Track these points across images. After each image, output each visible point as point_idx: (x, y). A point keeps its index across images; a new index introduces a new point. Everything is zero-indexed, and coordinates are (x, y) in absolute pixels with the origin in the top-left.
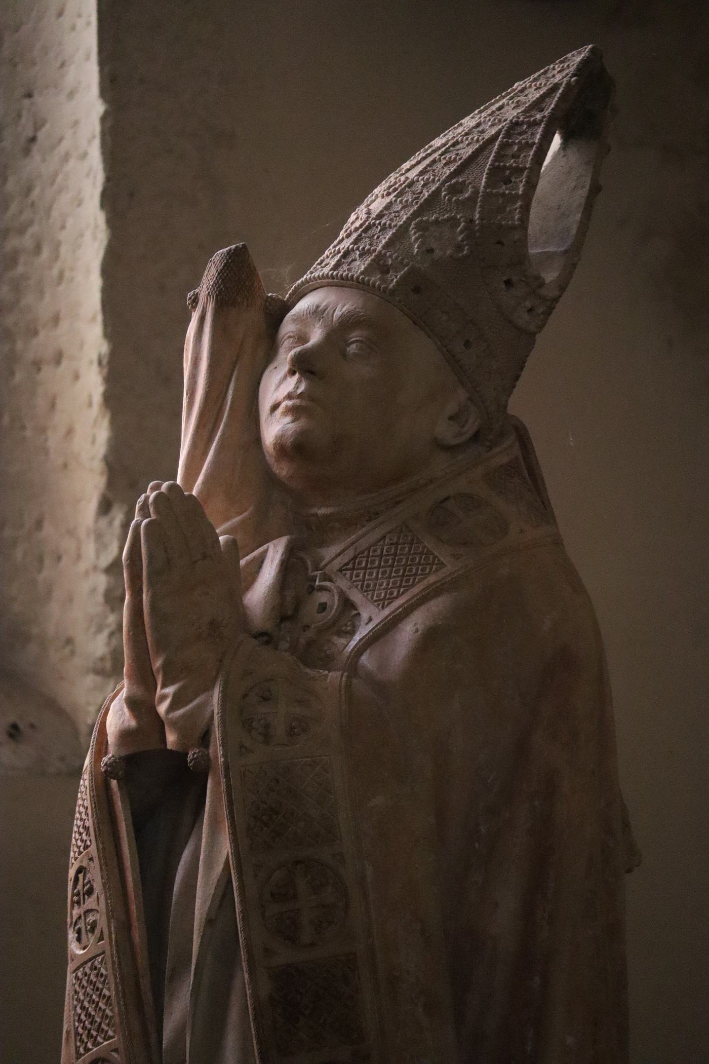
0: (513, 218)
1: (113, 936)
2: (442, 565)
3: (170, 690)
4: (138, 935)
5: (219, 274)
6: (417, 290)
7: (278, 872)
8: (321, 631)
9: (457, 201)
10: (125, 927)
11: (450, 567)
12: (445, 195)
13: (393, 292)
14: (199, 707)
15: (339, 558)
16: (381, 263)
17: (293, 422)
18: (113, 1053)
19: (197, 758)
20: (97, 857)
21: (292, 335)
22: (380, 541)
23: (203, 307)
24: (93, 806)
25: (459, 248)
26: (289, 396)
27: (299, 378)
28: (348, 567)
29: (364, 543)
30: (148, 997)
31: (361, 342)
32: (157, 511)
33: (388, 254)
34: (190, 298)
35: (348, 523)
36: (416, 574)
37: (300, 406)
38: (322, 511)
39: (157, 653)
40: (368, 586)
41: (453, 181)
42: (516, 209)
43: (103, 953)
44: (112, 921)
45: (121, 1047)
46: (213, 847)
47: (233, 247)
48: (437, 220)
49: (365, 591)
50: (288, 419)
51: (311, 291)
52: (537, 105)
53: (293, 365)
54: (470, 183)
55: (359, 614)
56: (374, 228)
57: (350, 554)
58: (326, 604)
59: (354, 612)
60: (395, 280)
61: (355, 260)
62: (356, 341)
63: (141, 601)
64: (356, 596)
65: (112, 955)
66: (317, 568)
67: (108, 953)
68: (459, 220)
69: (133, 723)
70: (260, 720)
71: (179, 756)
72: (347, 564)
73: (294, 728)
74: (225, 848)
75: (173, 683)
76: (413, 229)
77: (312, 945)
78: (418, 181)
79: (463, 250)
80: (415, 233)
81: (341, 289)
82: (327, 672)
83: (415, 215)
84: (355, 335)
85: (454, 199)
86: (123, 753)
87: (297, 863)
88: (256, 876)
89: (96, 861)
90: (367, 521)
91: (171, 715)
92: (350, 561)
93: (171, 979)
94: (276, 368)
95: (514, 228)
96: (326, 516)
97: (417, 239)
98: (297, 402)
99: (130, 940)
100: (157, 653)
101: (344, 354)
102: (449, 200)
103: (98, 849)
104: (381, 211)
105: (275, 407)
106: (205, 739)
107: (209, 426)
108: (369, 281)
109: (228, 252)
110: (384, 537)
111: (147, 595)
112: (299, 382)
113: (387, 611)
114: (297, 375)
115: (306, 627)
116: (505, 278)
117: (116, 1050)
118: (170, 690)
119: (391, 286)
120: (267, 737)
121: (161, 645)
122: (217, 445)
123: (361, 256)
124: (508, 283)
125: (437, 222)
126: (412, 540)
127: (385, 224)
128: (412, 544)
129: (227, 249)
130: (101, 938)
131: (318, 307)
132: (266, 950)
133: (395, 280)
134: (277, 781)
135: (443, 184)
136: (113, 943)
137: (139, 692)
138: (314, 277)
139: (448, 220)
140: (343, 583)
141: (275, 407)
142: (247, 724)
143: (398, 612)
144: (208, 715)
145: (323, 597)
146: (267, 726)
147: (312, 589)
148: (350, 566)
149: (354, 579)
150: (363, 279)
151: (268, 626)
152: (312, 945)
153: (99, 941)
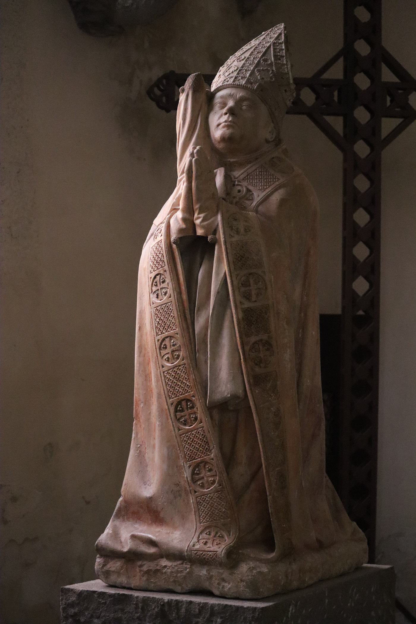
0: (285, 71)
1: (176, 296)
2: (279, 179)
3: (202, 215)
4: (185, 297)
5: (193, 82)
6: (262, 90)
7: (243, 277)
8: (240, 198)
9: (267, 64)
10: (180, 293)
11: (281, 180)
12: (263, 62)
13: (256, 90)
14: (213, 222)
15: (242, 175)
16: (250, 81)
17: (227, 130)
18: (176, 335)
19: (212, 238)
20: (168, 270)
21: (221, 102)
22: (255, 170)
23: (188, 92)
24: (167, 253)
25: (271, 78)
26: (226, 122)
27: (229, 116)
28: (246, 178)
29: (250, 171)
30: (188, 316)
31: (247, 105)
32: (197, 155)
33: (251, 78)
34: (181, 91)
35: (241, 165)
36: (271, 181)
37: (230, 125)
38: (232, 160)
39: (197, 203)
40: (254, 185)
41: (263, 58)
42: (285, 68)
43: (171, 302)
44: (175, 291)
45: (179, 332)
46: (218, 268)
47: (197, 73)
48: (263, 69)
49: (254, 186)
50: (225, 129)
51: (223, 89)
52: (278, 38)
53: (228, 111)
54: (269, 59)
55: (253, 194)
56: (242, 70)
57: (245, 174)
58: (240, 190)
59: (252, 193)
60: (255, 87)
61: (240, 80)
62: (245, 105)
63: (191, 185)
64: (250, 188)
65: (175, 303)
66: (235, 178)
67: (173, 302)
68: (269, 70)
69: (184, 226)
70: (235, 226)
71: (203, 238)
72: (245, 177)
73: (246, 229)
74: (225, 268)
75: (202, 213)
76: (256, 71)
77: (255, 301)
78: (250, 57)
79: (273, 79)
80: (257, 73)
81: (237, 88)
82: (246, 212)
83: (256, 67)
84: (245, 103)
85: (266, 63)
86: (180, 236)
87: (250, 274)
88: (237, 278)
89: (168, 272)
90: (247, 164)
91: (202, 224)
92: (246, 176)
93: (199, 310)
94: (215, 113)
95: (286, 74)
96: (234, 162)
97: (259, 75)
98: (229, 123)
99: (181, 297)
100: (197, 203)
101: (241, 109)
102: (264, 63)
103: (169, 267)
104: (242, 66)
105: (219, 125)
106: (215, 232)
107: (192, 131)
108: (248, 86)
109: (196, 75)
110: (256, 169)
111: (195, 183)
112: (229, 117)
113: (264, 193)
114: (228, 115)
115: (234, 197)
116: (285, 89)
117: (177, 334)
118: (202, 215)
119: (255, 88)
120: (238, 232)
121: (198, 200)
122: (196, 136)
123: (242, 78)
124: (285, 91)
125: (263, 70)
126: (266, 170)
127: (246, 69)
128: (266, 172)
129: (195, 74)
130: (170, 297)
131: (230, 93)
132: (241, 302)
133: (255, 87)
134: (243, 247)
135: (260, 59)
136: (176, 299)
137: (187, 216)
138: (224, 85)
139: (266, 70)
140: (245, 184)
141: (219, 125)
142: (231, 228)
143: (269, 193)
144: (216, 224)
145: (239, 188)
146: (238, 229)
147: (234, 185)
148: (246, 178)
149: (249, 182)
150: (246, 85)
151: (224, 196)
152: (255, 301)
153: (169, 298)
